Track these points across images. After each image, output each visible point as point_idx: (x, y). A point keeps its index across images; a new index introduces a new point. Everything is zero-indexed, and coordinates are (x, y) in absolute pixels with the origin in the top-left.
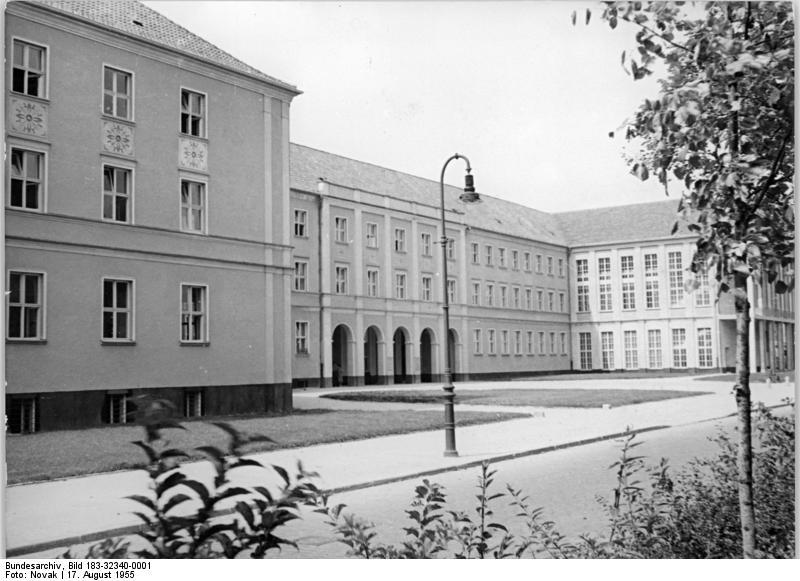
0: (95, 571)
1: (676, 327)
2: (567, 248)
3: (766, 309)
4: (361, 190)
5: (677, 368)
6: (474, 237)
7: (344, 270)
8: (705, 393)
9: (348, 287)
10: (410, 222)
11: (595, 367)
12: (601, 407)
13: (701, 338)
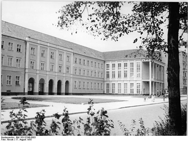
0: (22, 139)
1: (125, 83)
2: (104, 61)
3: (155, 79)
4: (50, 43)
5: (131, 94)
6: (75, 56)
7: (61, 67)
8: (124, 101)
9: (62, 71)
10: (56, 50)
11: (110, 93)
12: (81, 104)
13: (137, 86)
